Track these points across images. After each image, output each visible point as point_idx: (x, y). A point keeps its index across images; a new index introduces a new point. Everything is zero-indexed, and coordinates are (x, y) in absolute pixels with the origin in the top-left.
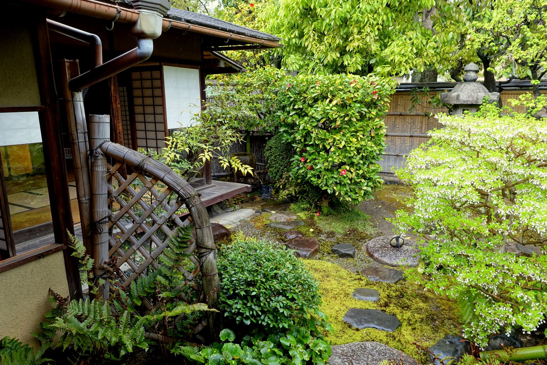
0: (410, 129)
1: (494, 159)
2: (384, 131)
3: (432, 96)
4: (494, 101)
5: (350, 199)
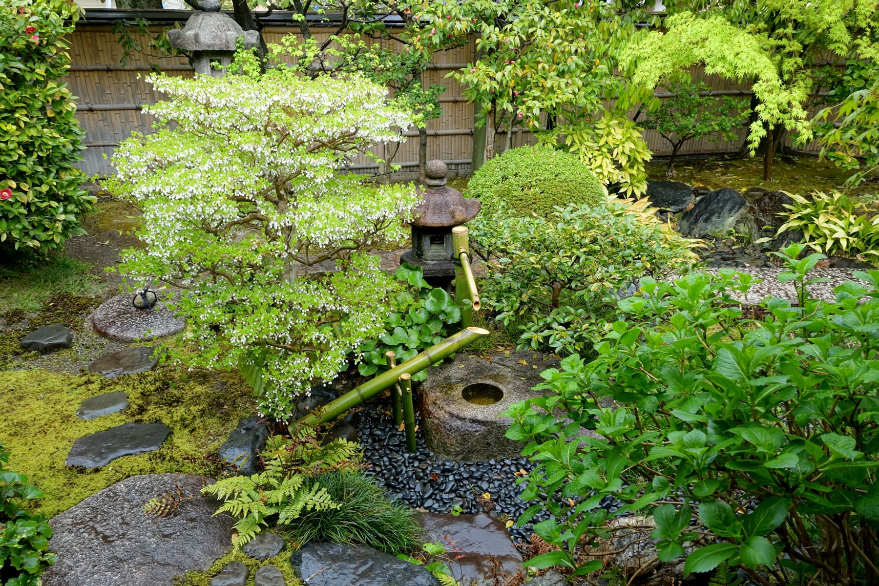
0: (133, 95)
1: (248, 147)
2: (72, 106)
3: (156, 35)
4: (253, 45)
5: (37, 244)
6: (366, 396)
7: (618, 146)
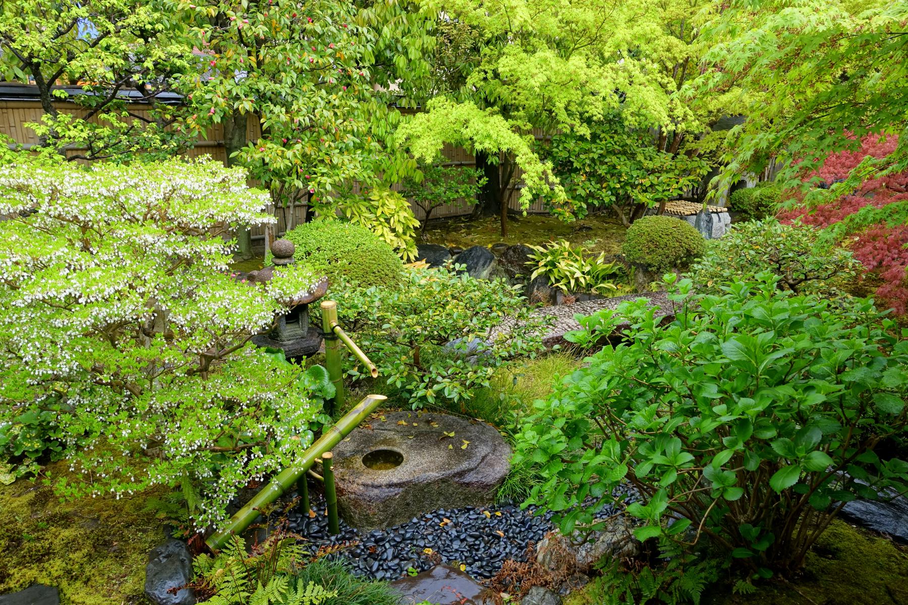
6: (285, 487)
7: (393, 215)
